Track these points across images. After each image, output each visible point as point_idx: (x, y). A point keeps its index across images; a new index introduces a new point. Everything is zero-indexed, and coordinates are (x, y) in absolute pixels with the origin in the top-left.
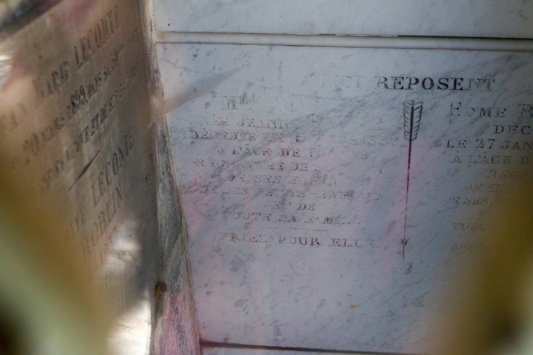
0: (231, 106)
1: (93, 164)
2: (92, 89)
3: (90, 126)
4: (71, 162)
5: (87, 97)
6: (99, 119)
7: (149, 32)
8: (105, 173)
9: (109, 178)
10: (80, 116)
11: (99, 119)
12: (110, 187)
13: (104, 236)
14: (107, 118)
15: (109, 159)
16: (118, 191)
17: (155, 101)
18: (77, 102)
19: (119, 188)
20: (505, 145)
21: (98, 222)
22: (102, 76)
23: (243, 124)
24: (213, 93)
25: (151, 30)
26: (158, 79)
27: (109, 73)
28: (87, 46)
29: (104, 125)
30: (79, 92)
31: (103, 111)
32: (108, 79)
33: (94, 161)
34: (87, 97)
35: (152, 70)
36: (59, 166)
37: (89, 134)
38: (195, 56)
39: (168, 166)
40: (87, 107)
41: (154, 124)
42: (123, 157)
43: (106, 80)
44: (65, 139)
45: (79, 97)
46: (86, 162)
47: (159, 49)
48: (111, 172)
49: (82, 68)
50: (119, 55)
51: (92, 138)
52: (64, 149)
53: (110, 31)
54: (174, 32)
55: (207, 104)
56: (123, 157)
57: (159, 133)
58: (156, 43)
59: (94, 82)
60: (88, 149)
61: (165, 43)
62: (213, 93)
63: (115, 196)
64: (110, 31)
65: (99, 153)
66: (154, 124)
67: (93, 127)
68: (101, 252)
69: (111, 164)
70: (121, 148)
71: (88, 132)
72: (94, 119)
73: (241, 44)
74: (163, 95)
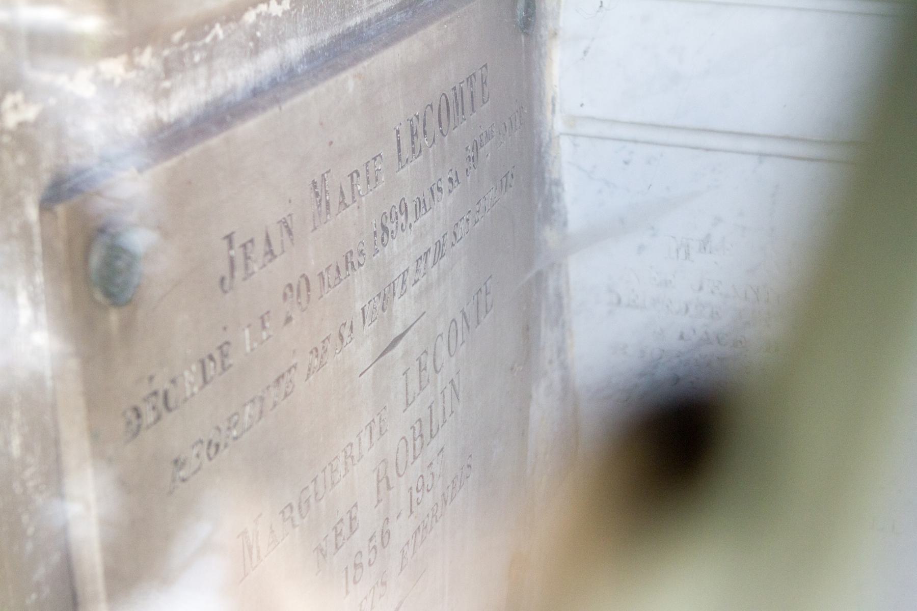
0: (682, 253)
1: (409, 333)
2: (421, 205)
3: (412, 268)
4: (368, 329)
5: (411, 219)
6: (431, 258)
7: (549, 114)
8: (431, 351)
9: (439, 363)
10: (395, 249)
11: (431, 258)
12: (439, 376)
13: (418, 461)
14: (445, 258)
15: (442, 328)
16: (453, 386)
17: (550, 235)
18: (391, 227)
19: (456, 382)
20: (225, 348)
21: (409, 436)
22: (445, 185)
23: (701, 288)
24: (653, 228)
25: (553, 111)
26: (559, 197)
27: (457, 180)
28: (420, 131)
29: (439, 269)
30: (397, 210)
31: (440, 245)
32: (455, 191)
33: (413, 328)
34: (411, 219)
35: (548, 181)
36: (346, 332)
37: (407, 283)
38: (626, 163)
39: (561, 350)
40: (409, 236)
41: (539, 274)
42: (468, 327)
43: (450, 191)
44: (361, 287)
45: (397, 218)
46: (398, 331)
47: (565, 144)
48: (443, 352)
49: (408, 167)
50: (481, 150)
51: (413, 290)
52: (358, 307)
53: (467, 107)
54: (593, 119)
55: (641, 248)
56: (468, 327)
57: (551, 291)
58: (561, 134)
59: (428, 194)
60: (404, 309)
61: (575, 136)
62: (653, 228)
63: (448, 392)
64: (467, 107)
65: (425, 316)
66: (539, 274)
67: (417, 271)
68: (411, 489)
69: (445, 336)
70: (465, 310)
71: (407, 278)
72: (420, 258)
73: (707, 150)
74: (565, 224)
